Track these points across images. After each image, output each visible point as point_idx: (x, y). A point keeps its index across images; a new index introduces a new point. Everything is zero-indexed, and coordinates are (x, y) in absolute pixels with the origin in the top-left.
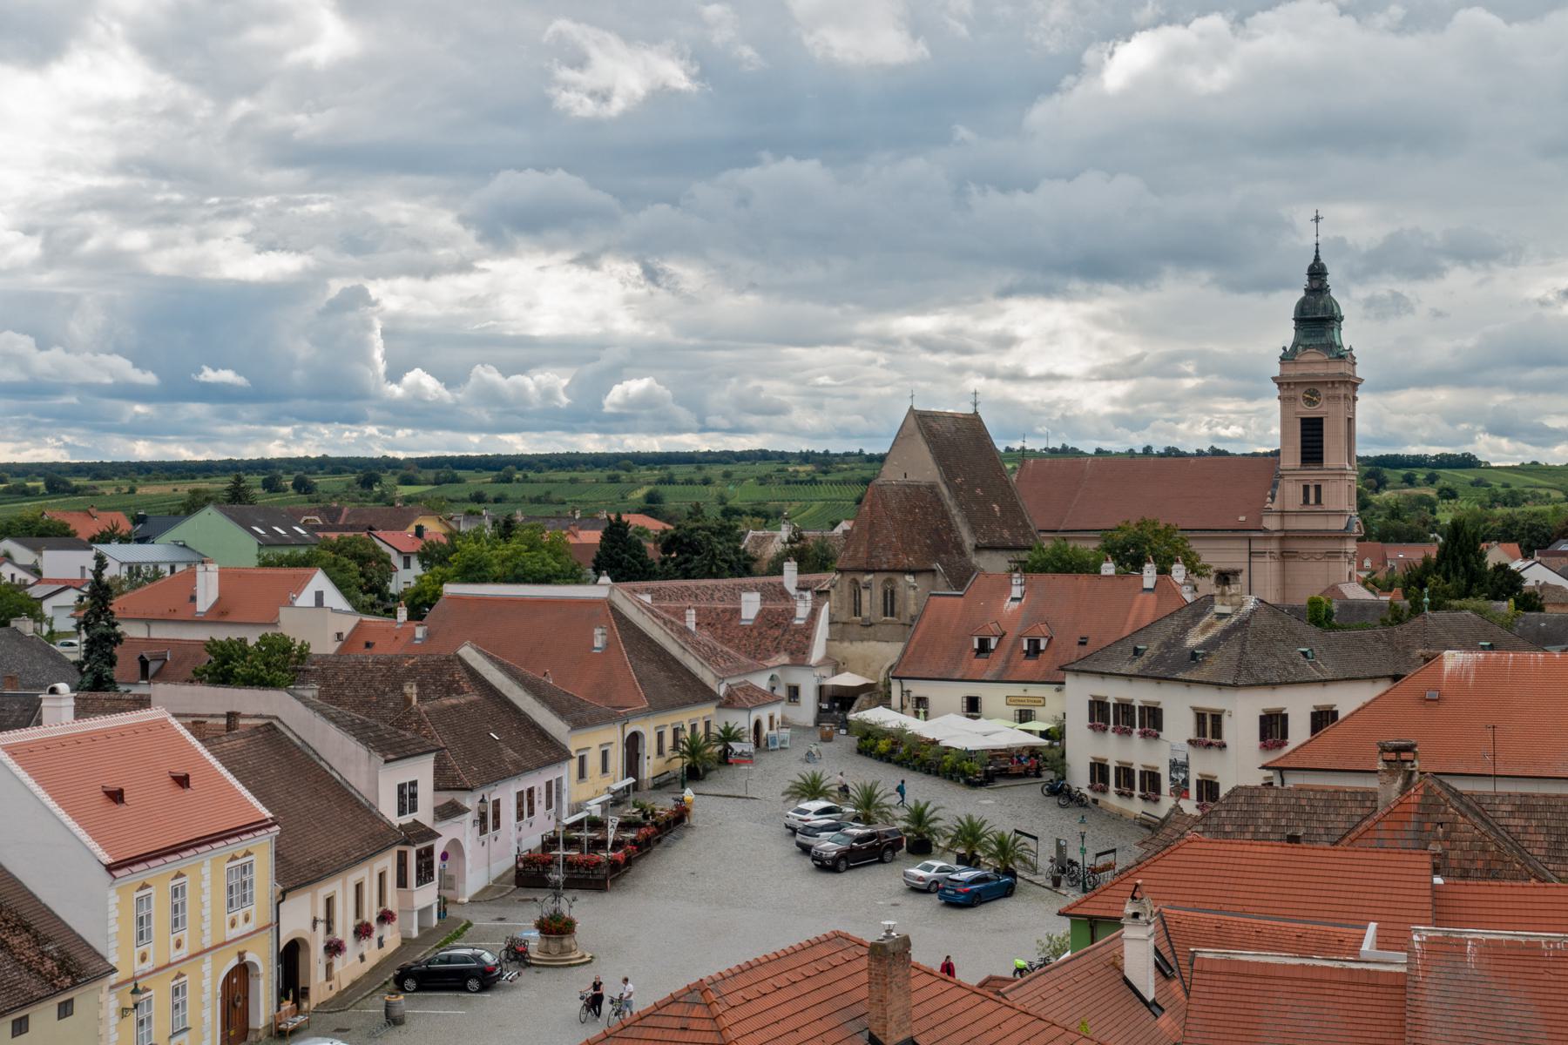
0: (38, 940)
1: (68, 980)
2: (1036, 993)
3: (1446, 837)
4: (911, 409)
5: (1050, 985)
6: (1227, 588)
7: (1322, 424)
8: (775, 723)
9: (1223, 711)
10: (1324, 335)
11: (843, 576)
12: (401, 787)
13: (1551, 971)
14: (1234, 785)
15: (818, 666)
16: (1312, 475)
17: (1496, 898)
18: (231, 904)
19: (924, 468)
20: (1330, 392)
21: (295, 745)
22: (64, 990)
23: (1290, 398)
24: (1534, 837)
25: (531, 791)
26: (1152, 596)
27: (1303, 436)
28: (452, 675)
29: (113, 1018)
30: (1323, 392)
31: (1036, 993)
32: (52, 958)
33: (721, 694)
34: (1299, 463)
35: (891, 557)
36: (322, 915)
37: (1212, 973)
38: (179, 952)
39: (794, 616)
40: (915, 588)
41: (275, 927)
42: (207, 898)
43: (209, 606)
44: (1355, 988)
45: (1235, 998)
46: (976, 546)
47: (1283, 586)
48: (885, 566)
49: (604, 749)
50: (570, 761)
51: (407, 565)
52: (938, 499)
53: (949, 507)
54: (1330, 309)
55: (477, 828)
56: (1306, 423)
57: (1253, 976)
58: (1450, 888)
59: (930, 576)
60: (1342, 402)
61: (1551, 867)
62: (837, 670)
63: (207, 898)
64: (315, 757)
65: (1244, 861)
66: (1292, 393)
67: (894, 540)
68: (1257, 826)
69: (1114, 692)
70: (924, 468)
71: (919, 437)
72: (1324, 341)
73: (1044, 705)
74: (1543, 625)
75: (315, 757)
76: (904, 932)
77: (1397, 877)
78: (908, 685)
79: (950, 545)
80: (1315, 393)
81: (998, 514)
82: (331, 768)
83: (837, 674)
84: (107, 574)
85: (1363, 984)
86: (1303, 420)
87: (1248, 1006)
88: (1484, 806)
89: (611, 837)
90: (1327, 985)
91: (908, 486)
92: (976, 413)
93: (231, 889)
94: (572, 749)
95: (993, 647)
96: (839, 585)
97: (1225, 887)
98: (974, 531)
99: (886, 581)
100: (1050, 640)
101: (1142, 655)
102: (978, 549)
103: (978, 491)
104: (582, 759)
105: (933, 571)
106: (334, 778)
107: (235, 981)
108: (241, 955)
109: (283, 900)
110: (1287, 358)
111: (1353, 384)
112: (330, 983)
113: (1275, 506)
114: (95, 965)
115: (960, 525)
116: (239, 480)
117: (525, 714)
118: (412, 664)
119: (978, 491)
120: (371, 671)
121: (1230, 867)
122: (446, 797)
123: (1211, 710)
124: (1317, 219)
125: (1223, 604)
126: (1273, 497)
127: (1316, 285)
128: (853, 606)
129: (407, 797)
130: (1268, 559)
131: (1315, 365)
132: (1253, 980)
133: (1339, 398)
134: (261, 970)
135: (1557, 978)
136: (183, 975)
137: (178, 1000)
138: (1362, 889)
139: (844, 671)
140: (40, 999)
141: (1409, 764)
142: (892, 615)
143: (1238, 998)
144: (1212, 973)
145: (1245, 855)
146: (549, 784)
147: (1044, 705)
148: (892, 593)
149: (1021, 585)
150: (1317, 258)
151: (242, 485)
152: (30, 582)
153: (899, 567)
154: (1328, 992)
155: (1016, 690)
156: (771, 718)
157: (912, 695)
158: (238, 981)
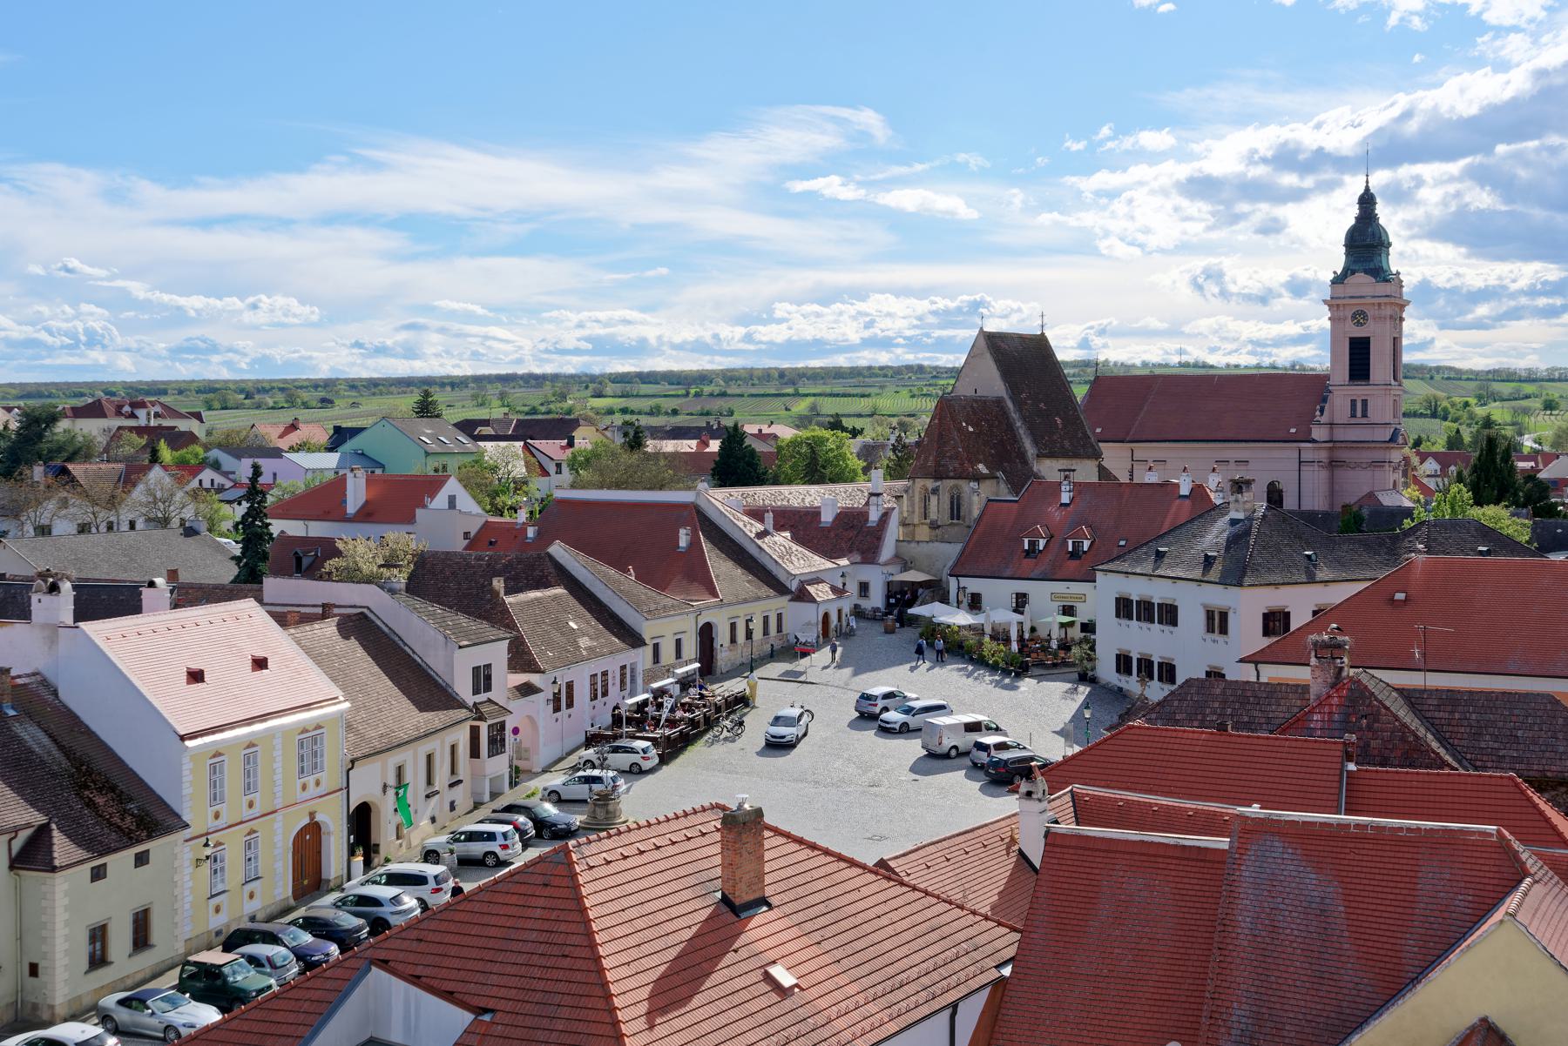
0: (121, 798)
1: (144, 834)
2: (921, 861)
3: (1369, 728)
5: (939, 854)
6: (1240, 495)
7: (1350, 375)
8: (844, 616)
12: (476, 670)
13: (1356, 851)
14: (1187, 677)
15: (886, 564)
16: (1359, 391)
17: (1487, 788)
18: (302, 771)
19: (992, 384)
21: (383, 632)
22: (139, 841)
24: (1456, 729)
25: (605, 674)
26: (1187, 502)
28: (542, 571)
29: (187, 869)
31: (921, 861)
32: (132, 815)
33: (793, 589)
34: (1347, 378)
36: (392, 781)
37: (1062, 846)
38: (252, 811)
39: (867, 520)
41: (345, 791)
42: (278, 765)
43: (357, 508)
44: (1185, 862)
45: (1080, 870)
47: (1332, 493)
48: (952, 474)
49: (678, 637)
50: (644, 648)
51: (559, 472)
52: (1004, 412)
54: (1378, 235)
55: (551, 706)
57: (1097, 850)
58: (1362, 775)
59: (995, 481)
60: (1388, 322)
61: (1469, 756)
62: (906, 567)
63: (278, 765)
64: (400, 642)
65: (1176, 747)
68: (1204, 715)
69: (1137, 589)
70: (992, 384)
71: (988, 356)
72: (1372, 266)
74: (1559, 531)
75: (400, 642)
76: (757, 805)
77: (1220, 763)
78: (964, 581)
79: (1014, 455)
81: (1060, 426)
82: (414, 652)
83: (905, 571)
84: (261, 480)
85: (1193, 860)
86: (1351, 339)
87: (1090, 877)
88: (1413, 700)
89: (664, 716)
90: (1160, 860)
91: (976, 401)
92: (1043, 334)
93: (302, 759)
94: (647, 637)
95: (1085, 549)
97: (1157, 769)
100: (1050, 538)
103: (1042, 405)
104: (656, 647)
105: (997, 478)
106: (415, 661)
107: (308, 837)
108: (312, 815)
109: (352, 768)
110: (1338, 280)
112: (400, 841)
113: (1324, 419)
114: (170, 821)
115: (1023, 436)
116: (427, 394)
117: (606, 606)
118: (509, 561)
119: (1042, 405)
120: (474, 567)
121: (1163, 752)
122: (521, 678)
125: (1237, 510)
126: (1322, 411)
129: (483, 678)
130: (1316, 468)
132: (1097, 854)
133: (1385, 318)
134: (332, 828)
135: (1360, 857)
136: (255, 832)
137: (250, 854)
138: (1279, 774)
139: (911, 568)
140: (116, 850)
141: (1339, 661)
143: (1082, 870)
144: (1062, 846)
145: (1178, 741)
146: (623, 668)
149: (1070, 491)
151: (430, 399)
152: (227, 487)
154: (1161, 866)
155: (1059, 587)
156: (840, 611)
157: (968, 591)
158: (309, 842)
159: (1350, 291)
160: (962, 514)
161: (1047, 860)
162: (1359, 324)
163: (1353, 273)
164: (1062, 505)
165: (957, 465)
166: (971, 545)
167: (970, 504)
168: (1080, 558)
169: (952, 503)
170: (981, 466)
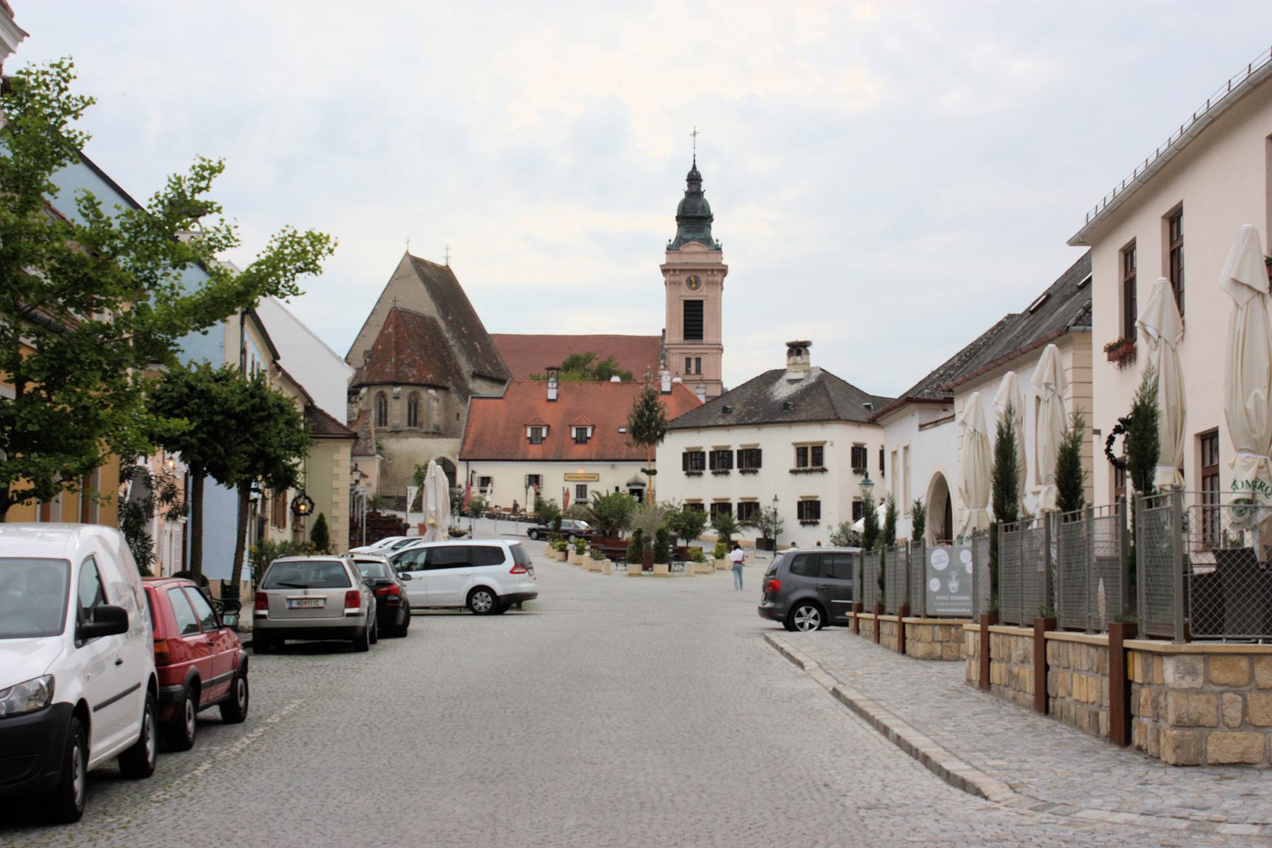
4: (407, 254)
7: (702, 306)
9: (825, 442)
11: (369, 390)
16: (693, 349)
20: (710, 279)
23: (675, 283)
30: (703, 278)
40: (438, 400)
48: (411, 380)
56: (687, 303)
66: (677, 279)
69: (707, 441)
72: (702, 236)
78: (474, 466)
80: (697, 282)
92: (447, 266)
100: (594, 427)
101: (730, 413)
102: (477, 376)
111: (724, 271)
119: (463, 329)
123: (811, 443)
124: (695, 134)
131: (694, 254)
142: (415, 425)
148: (416, 406)
150: (694, 167)
160: (419, 420)
161: (698, 328)
163: (687, 241)
165: (415, 372)
166: (469, 441)
168: (585, 442)
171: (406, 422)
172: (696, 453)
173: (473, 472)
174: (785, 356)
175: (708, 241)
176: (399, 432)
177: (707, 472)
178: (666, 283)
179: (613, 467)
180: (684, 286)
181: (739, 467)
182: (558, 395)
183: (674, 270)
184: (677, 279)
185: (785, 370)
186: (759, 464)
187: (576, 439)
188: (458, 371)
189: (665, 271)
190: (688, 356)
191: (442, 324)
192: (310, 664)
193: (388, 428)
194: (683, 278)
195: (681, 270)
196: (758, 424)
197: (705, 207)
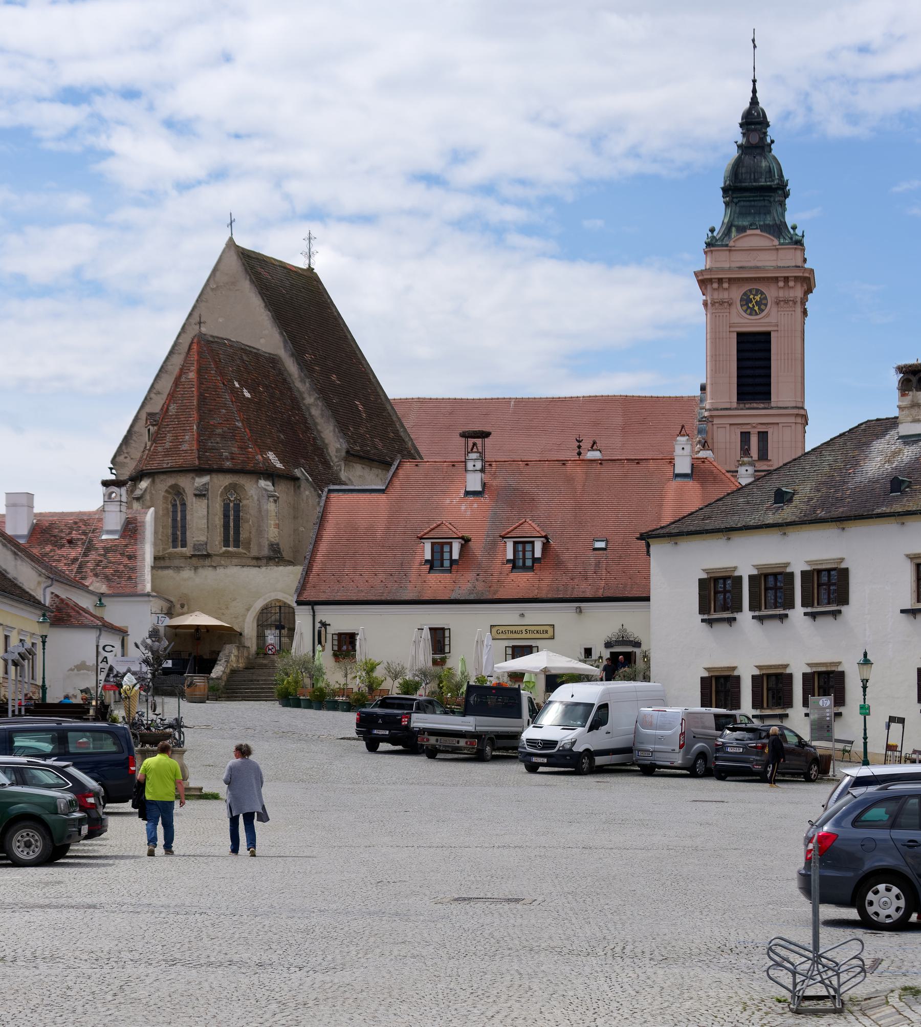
7: (769, 342)
10: (769, 212)
11: (153, 482)
20: (781, 294)
23: (722, 303)
27: (739, 360)
30: (772, 293)
34: (735, 400)
35: (235, 450)
46: (348, 452)
48: (228, 464)
53: (301, 393)
66: (725, 295)
67: (239, 424)
72: (769, 221)
73: (553, 638)
78: (325, 614)
86: (740, 335)
92: (310, 269)
96: (148, 497)
98: (342, 427)
99: (227, 489)
101: (790, 500)
102: (351, 456)
105: (295, 479)
115: (319, 420)
119: (334, 377)
127: (755, 139)
128: (170, 531)
133: (795, 302)
142: (237, 545)
147: (553, 638)
150: (754, 101)
153: (250, 466)
157: (331, 630)
159: (739, 260)
160: (243, 535)
162: (752, 312)
164: (467, 493)
167: (261, 515)
169: (226, 516)
170: (271, 456)
171: (218, 537)
172: (725, 579)
173: (324, 625)
174: (897, 393)
175: (779, 229)
176: (208, 556)
177: (746, 616)
178: (705, 304)
179: (580, 611)
180: (738, 308)
181: (752, 608)
182: (484, 485)
183: (720, 281)
184: (725, 295)
185: (896, 418)
186: (844, 599)
187: (513, 562)
188: (320, 451)
189: (704, 282)
190: (746, 429)
191: (291, 367)
192: (566, 779)
193: (188, 551)
194: (736, 294)
195: (731, 281)
196: (841, 520)
197: (774, 172)
